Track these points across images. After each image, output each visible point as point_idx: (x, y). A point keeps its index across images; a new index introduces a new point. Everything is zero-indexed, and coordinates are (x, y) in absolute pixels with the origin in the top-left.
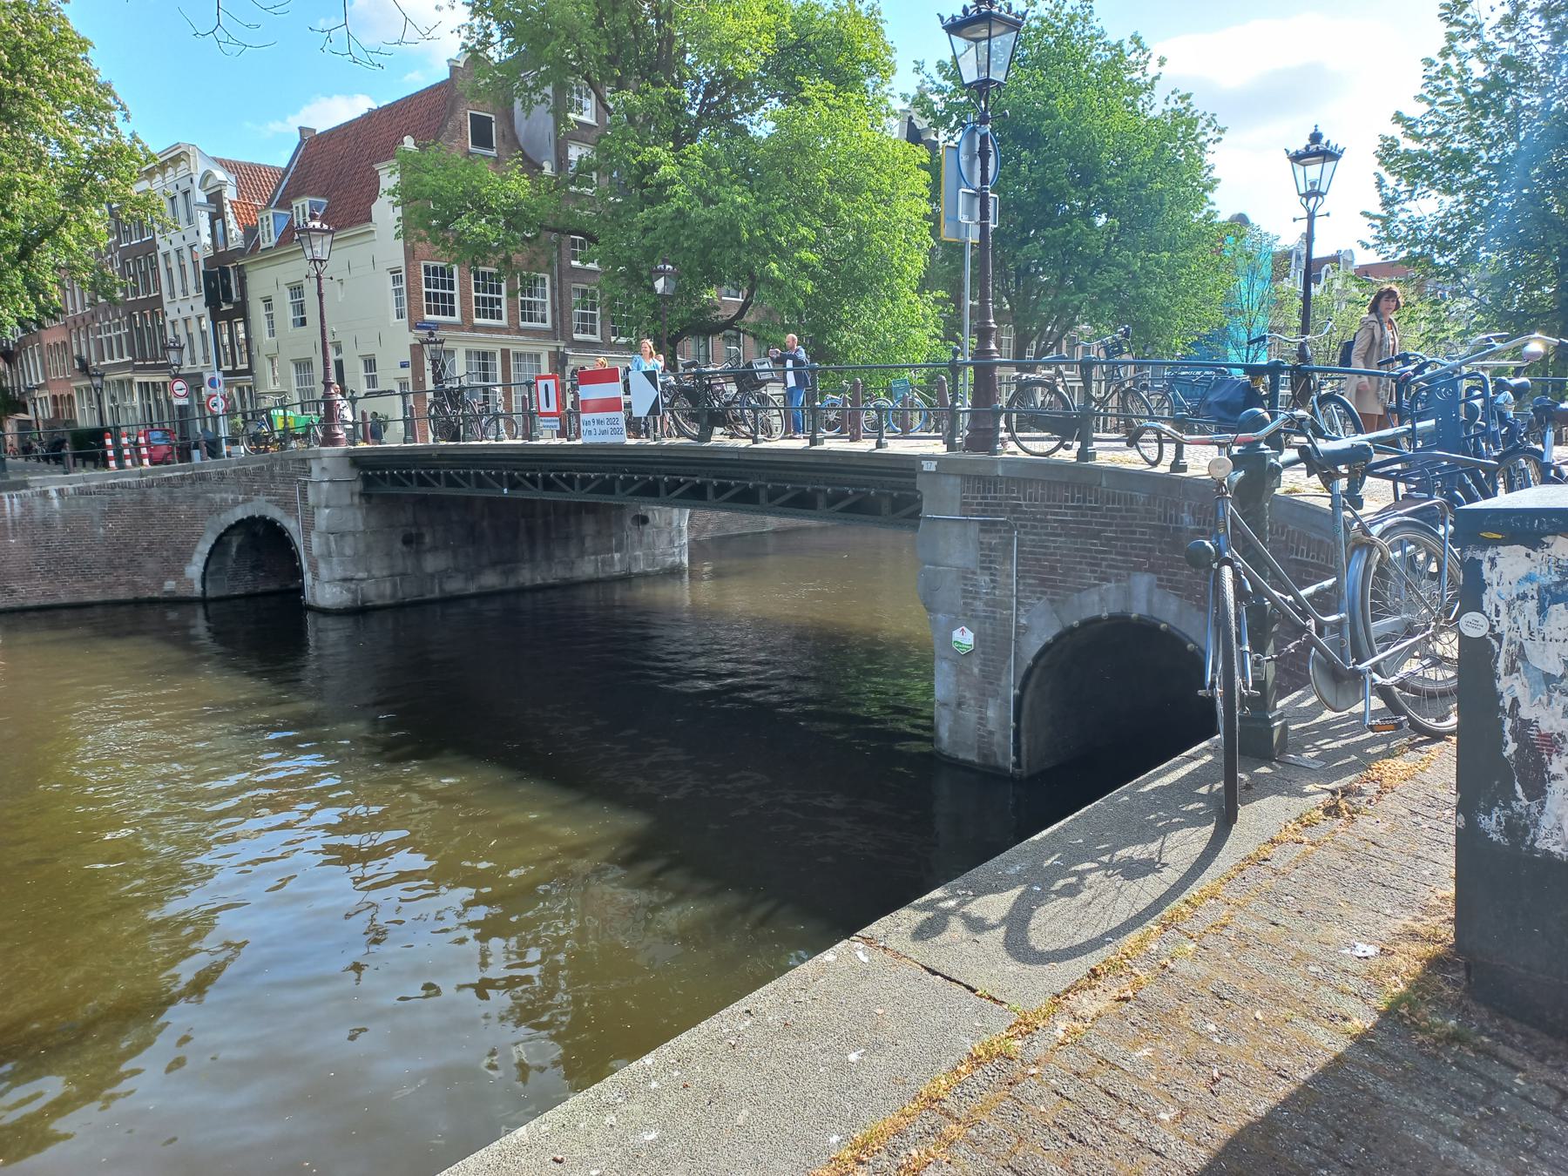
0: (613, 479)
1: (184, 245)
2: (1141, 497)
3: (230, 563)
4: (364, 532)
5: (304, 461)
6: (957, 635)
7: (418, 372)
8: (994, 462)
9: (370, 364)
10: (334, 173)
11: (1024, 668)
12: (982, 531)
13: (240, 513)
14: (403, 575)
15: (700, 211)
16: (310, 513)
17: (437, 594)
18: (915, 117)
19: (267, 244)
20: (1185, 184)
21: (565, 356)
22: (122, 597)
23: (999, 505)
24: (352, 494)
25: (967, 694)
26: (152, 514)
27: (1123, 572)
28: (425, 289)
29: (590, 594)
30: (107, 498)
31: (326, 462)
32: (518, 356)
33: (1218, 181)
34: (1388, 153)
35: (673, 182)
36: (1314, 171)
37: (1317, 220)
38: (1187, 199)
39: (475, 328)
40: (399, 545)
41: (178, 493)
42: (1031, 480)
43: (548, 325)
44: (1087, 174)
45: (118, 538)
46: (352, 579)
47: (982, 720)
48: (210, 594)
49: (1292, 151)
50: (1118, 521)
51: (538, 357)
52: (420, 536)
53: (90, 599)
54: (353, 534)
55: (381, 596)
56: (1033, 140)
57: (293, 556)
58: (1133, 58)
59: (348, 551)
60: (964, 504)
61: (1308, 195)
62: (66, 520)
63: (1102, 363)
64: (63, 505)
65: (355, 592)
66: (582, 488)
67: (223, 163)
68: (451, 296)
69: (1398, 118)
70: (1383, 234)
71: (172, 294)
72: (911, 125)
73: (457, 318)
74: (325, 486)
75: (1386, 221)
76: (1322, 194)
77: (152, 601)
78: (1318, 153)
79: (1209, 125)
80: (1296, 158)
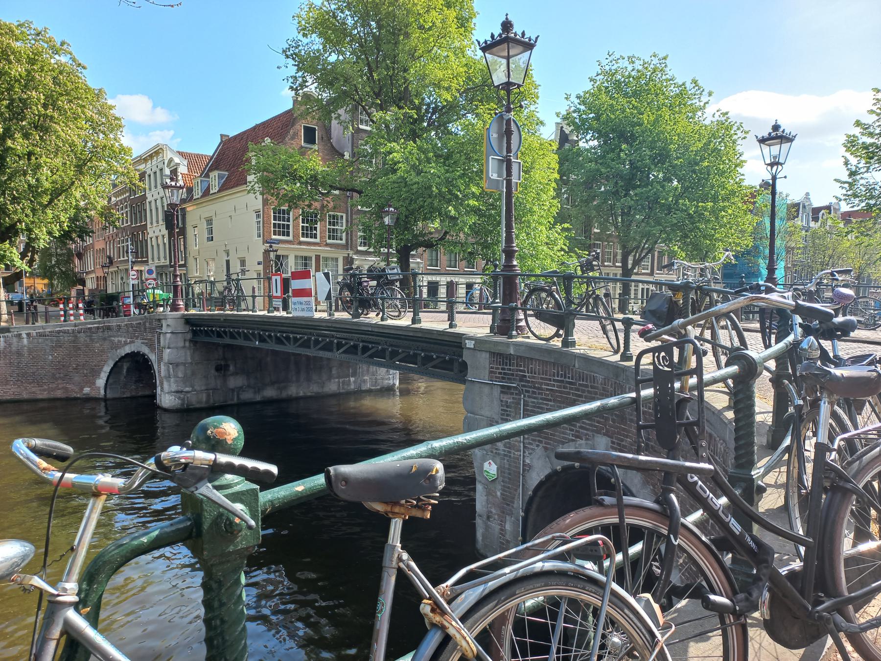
0: (309, 340)
1: (158, 197)
2: (600, 378)
3: (122, 378)
4: (191, 363)
5: (159, 320)
6: (486, 466)
8: (508, 345)
9: (243, 262)
10: (230, 160)
11: (527, 498)
12: (502, 392)
13: (127, 350)
14: (214, 389)
15: (413, 178)
16: (161, 352)
17: (235, 401)
18: (565, 126)
19: (197, 197)
20: (724, 163)
21: (352, 259)
22: (59, 396)
23: (513, 375)
24: (185, 340)
25: (494, 511)
26: (79, 349)
27: (590, 433)
28: (273, 222)
29: (333, 402)
30: (55, 339)
31: (170, 322)
32: (326, 259)
33: (745, 161)
34: (851, 144)
35: (399, 162)
36: (775, 149)
37: (778, 181)
38: (725, 172)
39: (300, 243)
40: (213, 371)
41: (95, 336)
42: (532, 359)
43: (344, 242)
44: (662, 157)
45: (59, 362)
46: (182, 392)
47: (503, 531)
48: (109, 396)
49: (760, 137)
50: (586, 394)
51: (337, 259)
52: (227, 367)
53: (40, 397)
54: (184, 364)
55: (200, 402)
56: (630, 139)
57: (152, 376)
58: (693, 91)
59: (180, 375)
60: (491, 372)
61: (772, 165)
62: (30, 351)
63: (578, 277)
64: (29, 342)
65: (183, 400)
66: (294, 344)
67: (181, 154)
68: (288, 226)
69: (858, 123)
70: (849, 193)
71: (152, 223)
72: (562, 131)
73: (291, 238)
74: (168, 335)
75: (851, 185)
76: (781, 164)
77: (76, 399)
78: (777, 137)
79: (738, 129)
80: (762, 141)
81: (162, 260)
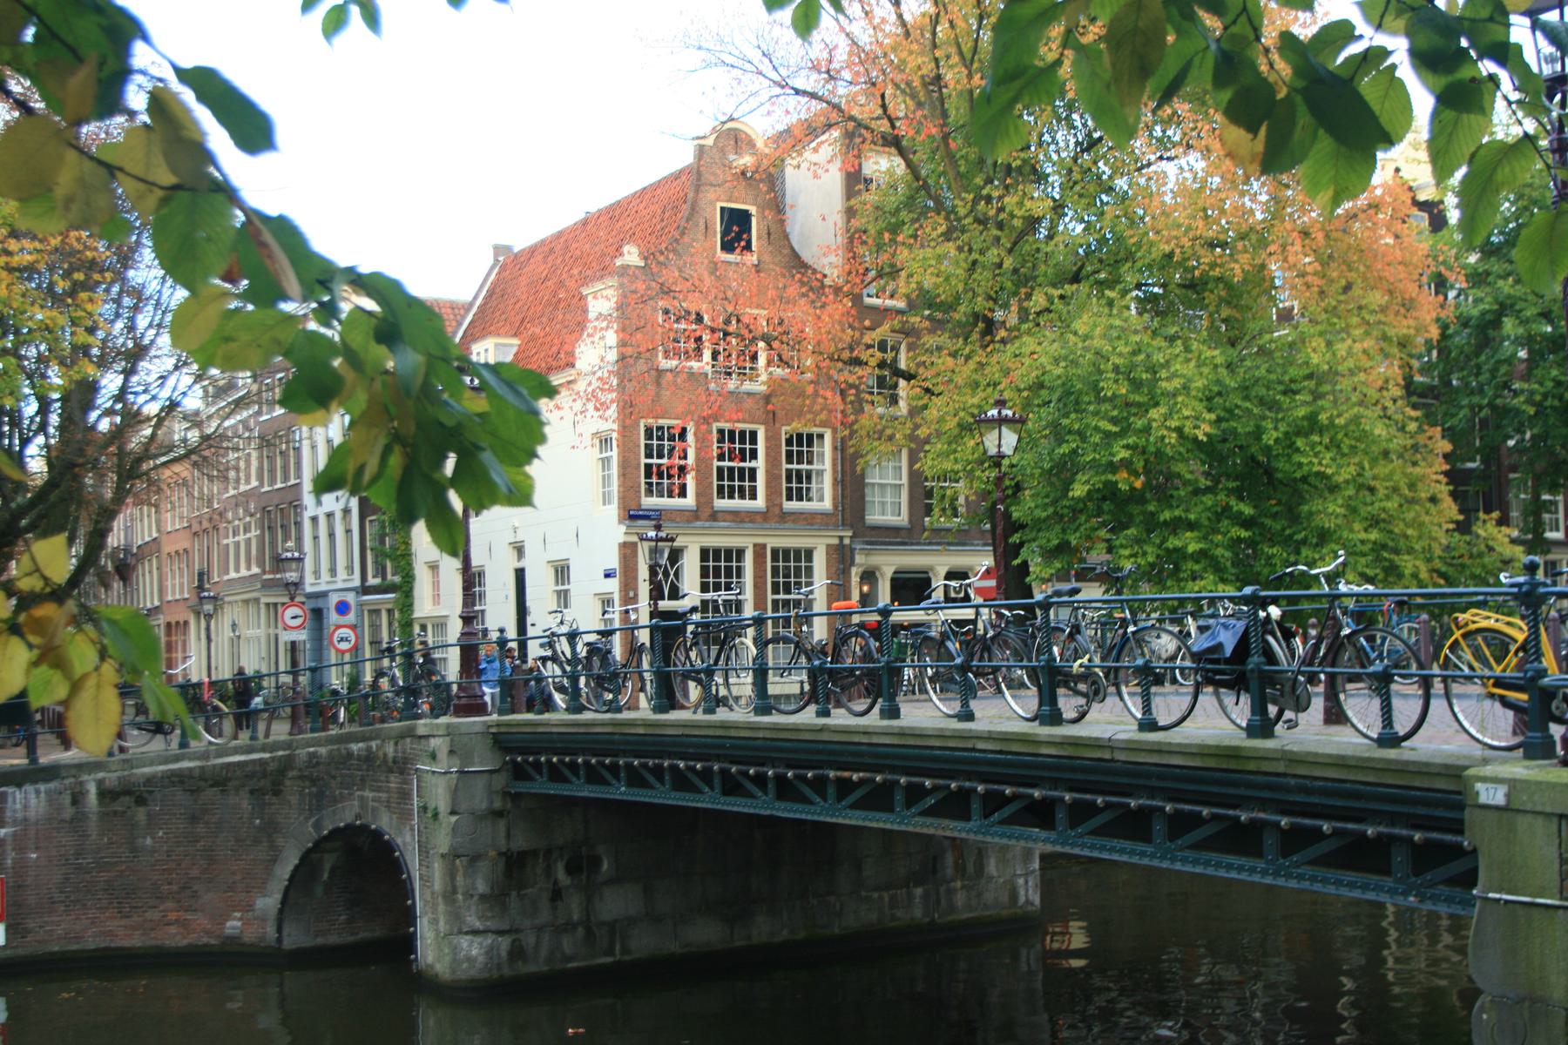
3: (319, 890)
7: (629, 585)
9: (562, 572)
28: (644, 461)
52: (595, 862)
68: (753, 471)
81: (342, 573)
